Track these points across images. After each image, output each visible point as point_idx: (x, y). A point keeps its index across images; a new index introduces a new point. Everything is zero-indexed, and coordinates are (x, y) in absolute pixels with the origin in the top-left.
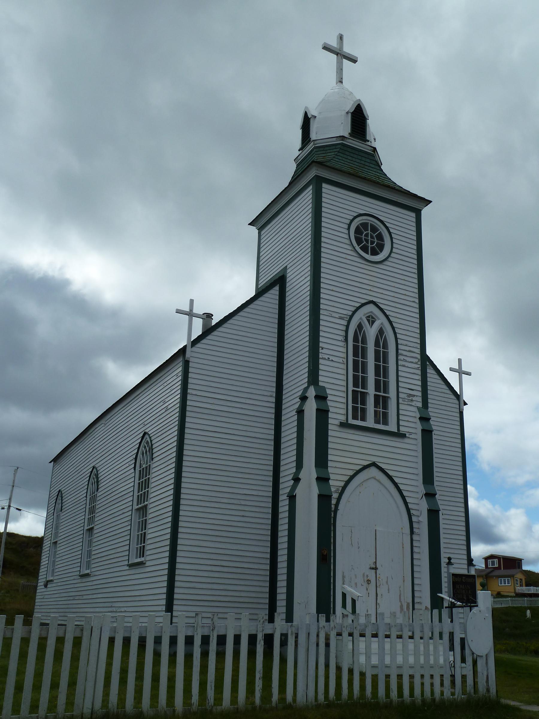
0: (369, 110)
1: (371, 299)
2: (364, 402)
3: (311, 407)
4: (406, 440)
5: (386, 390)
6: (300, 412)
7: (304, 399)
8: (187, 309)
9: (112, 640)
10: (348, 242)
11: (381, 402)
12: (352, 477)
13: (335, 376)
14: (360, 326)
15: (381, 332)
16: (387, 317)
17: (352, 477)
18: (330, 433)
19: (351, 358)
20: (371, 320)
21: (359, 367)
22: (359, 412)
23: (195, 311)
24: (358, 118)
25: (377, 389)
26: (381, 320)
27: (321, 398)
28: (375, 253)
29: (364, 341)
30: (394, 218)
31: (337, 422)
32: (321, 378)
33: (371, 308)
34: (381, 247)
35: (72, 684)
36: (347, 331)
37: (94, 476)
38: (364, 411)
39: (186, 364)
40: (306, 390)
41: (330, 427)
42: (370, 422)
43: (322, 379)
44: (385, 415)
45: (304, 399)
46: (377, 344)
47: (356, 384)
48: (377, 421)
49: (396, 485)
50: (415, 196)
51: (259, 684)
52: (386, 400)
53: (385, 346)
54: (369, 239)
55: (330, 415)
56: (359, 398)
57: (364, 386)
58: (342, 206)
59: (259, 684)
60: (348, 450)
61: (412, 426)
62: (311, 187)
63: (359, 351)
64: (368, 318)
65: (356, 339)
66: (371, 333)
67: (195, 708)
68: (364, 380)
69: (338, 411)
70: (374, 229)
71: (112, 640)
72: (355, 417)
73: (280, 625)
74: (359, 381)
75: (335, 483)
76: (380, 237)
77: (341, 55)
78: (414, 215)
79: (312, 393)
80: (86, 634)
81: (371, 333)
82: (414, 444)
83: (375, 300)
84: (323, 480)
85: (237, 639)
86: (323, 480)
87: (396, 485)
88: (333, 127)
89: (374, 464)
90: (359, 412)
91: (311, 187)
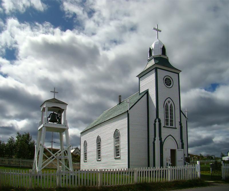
0: (166, 47)
1: (169, 97)
2: (168, 121)
3: (157, 123)
4: (177, 129)
5: (172, 118)
6: (155, 125)
7: (155, 121)
8: (54, 91)
9: (138, 172)
10: (163, 83)
11: (172, 121)
12: (166, 138)
13: (162, 116)
14: (167, 103)
15: (171, 104)
16: (172, 101)
17: (166, 138)
18: (162, 129)
19: (165, 111)
20: (169, 102)
21: (167, 113)
22: (167, 124)
23: (55, 91)
24: (164, 49)
25: (171, 118)
26: (171, 102)
27: (159, 121)
28: (169, 85)
29: (168, 107)
30: (173, 76)
31: (163, 126)
32: (159, 117)
33: (169, 99)
34: (171, 84)
35: (133, 179)
36: (164, 105)
37: (99, 140)
38: (168, 123)
39: (128, 115)
40: (156, 119)
41: (162, 128)
42: (169, 126)
43: (160, 117)
44: (172, 124)
45: (155, 121)
46: (170, 108)
47: (166, 118)
48: (171, 126)
49: (175, 139)
50: (178, 70)
51: (179, 178)
52: (172, 120)
53: (172, 108)
54: (168, 82)
55: (161, 125)
56: (167, 120)
57: (168, 118)
58: (162, 74)
59: (179, 178)
60: (165, 132)
61: (178, 126)
62: (154, 70)
63: (167, 110)
64: (168, 102)
65: (166, 107)
66: (169, 105)
67: (194, 179)
68: (168, 116)
69: (163, 124)
70: (169, 79)
71: (138, 172)
72: (171, 126)
73: (164, 169)
74: (167, 117)
75: (163, 140)
76: (170, 81)
77: (158, 31)
78: (177, 75)
79: (157, 120)
80: (134, 171)
81: (169, 105)
82: (178, 130)
83: (170, 97)
84: (161, 139)
85: (158, 171)
86: (161, 139)
87: (175, 139)
88: (157, 53)
89: (170, 135)
90: (167, 124)
91: (154, 70)
